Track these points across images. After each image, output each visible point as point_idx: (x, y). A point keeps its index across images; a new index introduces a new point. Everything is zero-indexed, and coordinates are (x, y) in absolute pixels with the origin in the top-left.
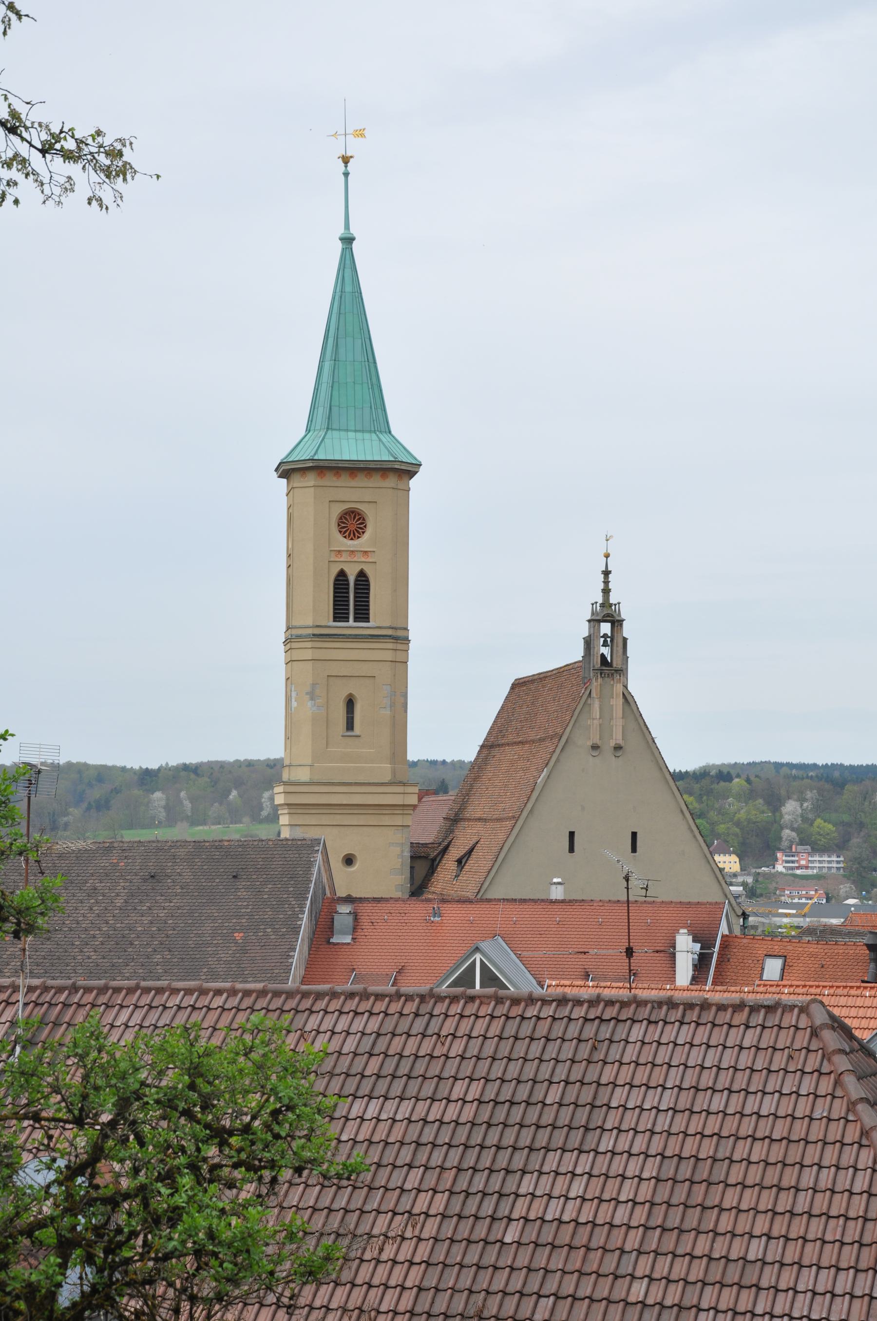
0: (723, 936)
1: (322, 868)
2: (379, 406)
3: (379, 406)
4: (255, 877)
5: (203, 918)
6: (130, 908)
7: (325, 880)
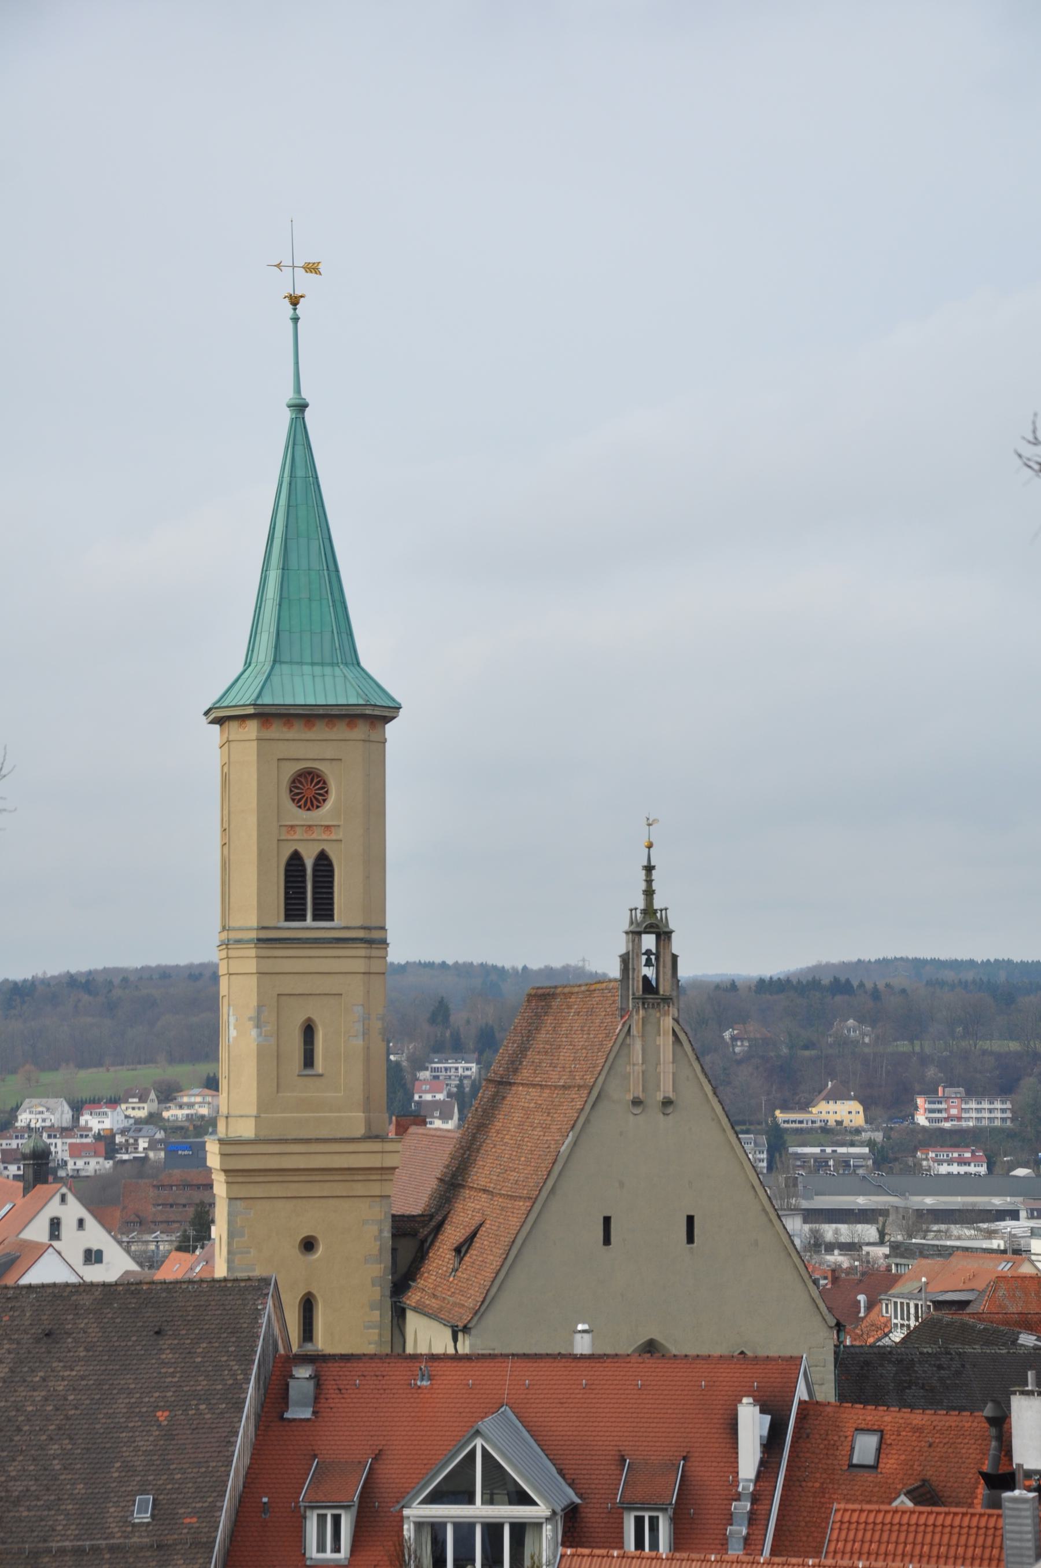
0: (801, 1402)
1: (273, 1317)
2: (343, 629)
3: (343, 629)
4: (184, 1332)
5: (115, 1392)
6: (17, 1379)
7: (277, 1332)
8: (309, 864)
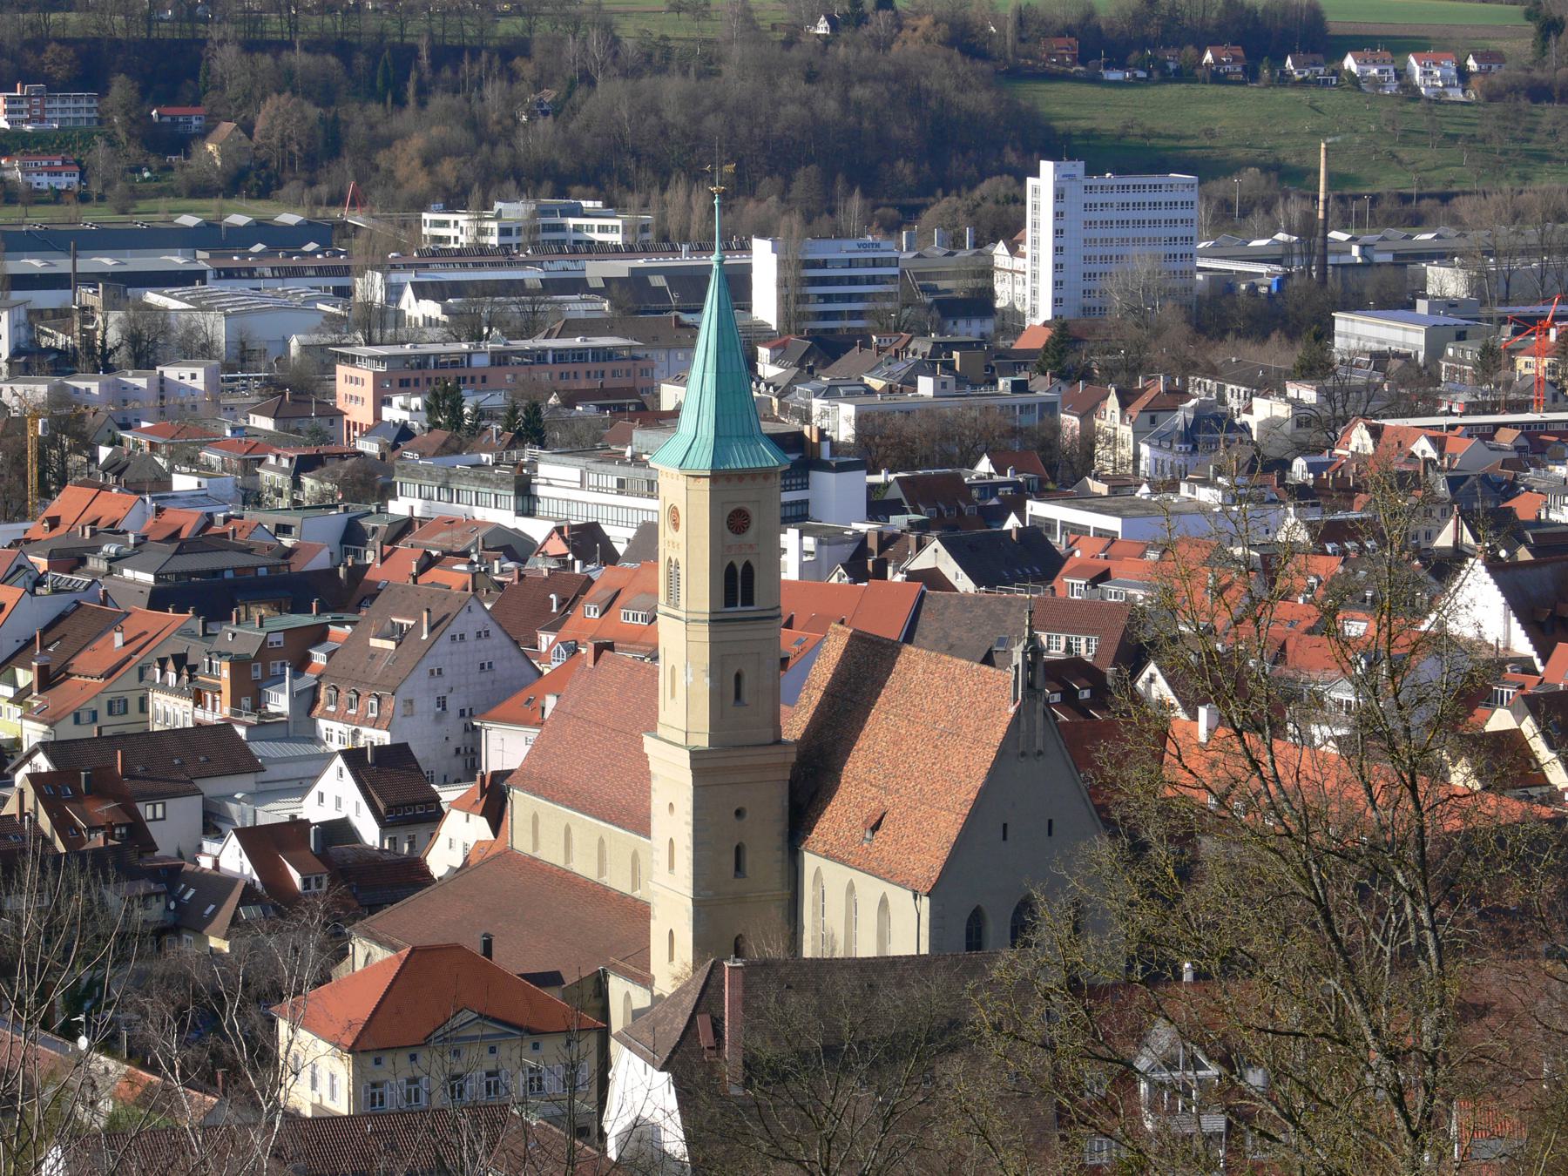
8: (740, 569)
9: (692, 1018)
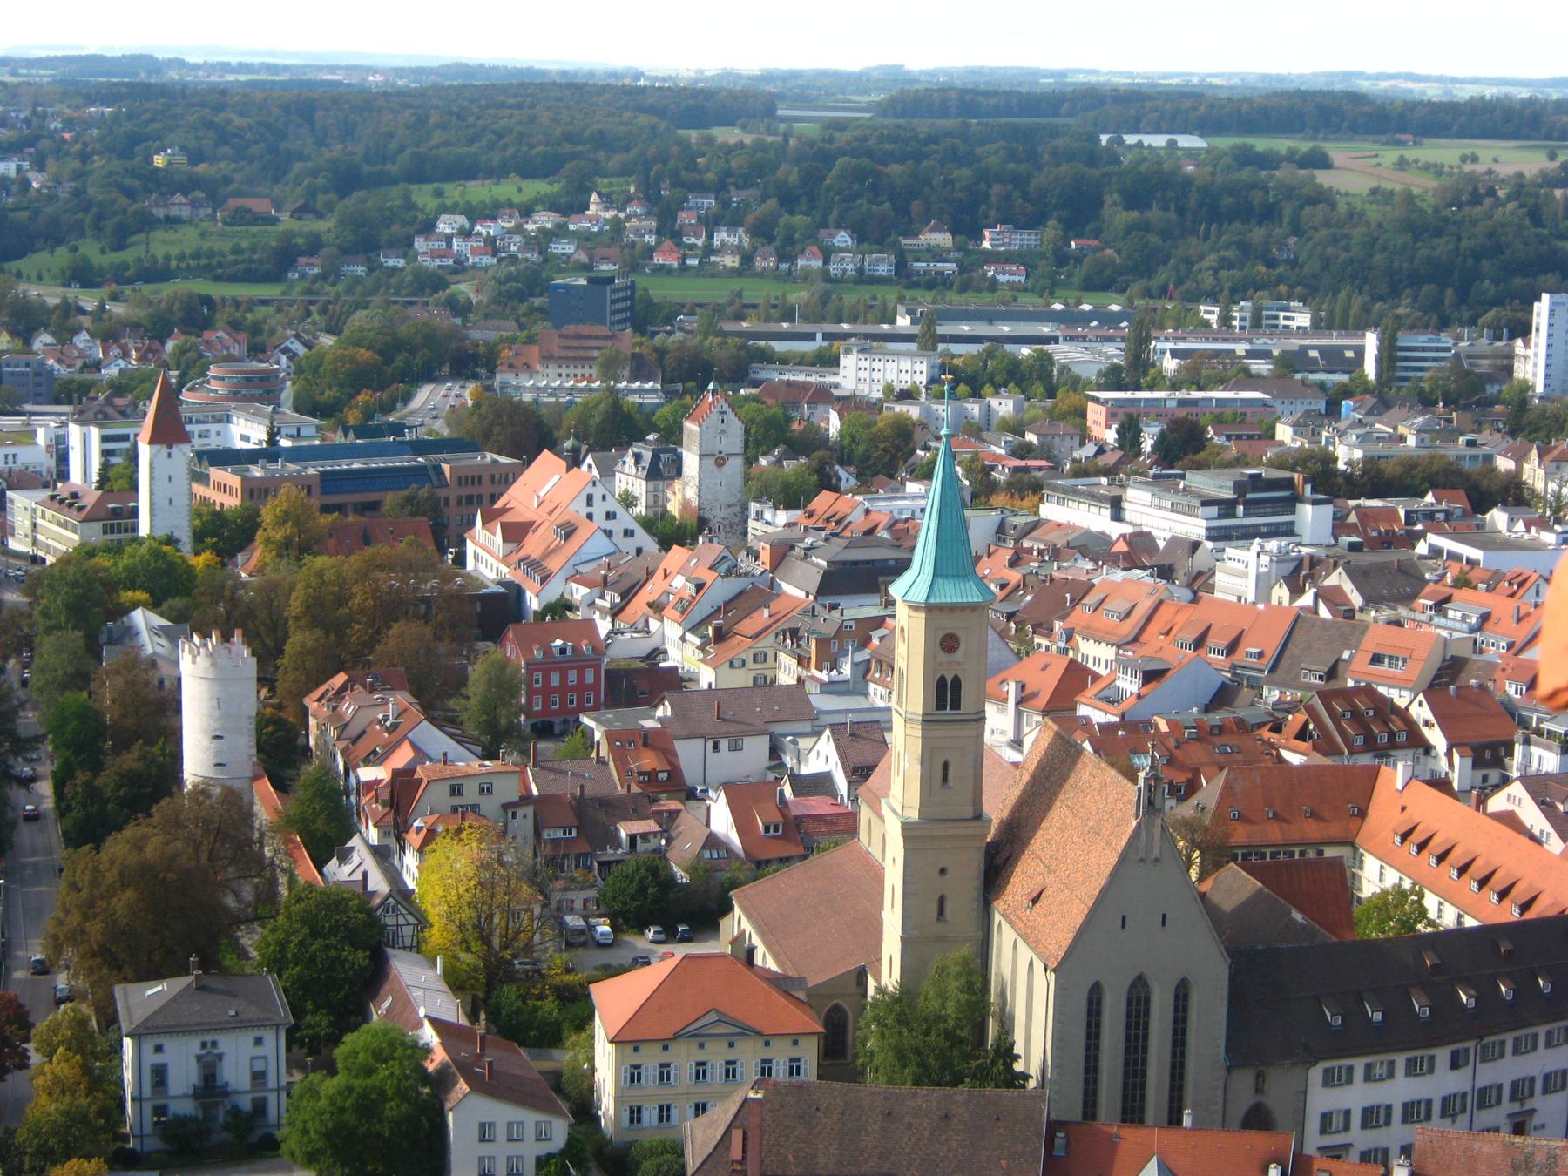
9: (728, 1131)
